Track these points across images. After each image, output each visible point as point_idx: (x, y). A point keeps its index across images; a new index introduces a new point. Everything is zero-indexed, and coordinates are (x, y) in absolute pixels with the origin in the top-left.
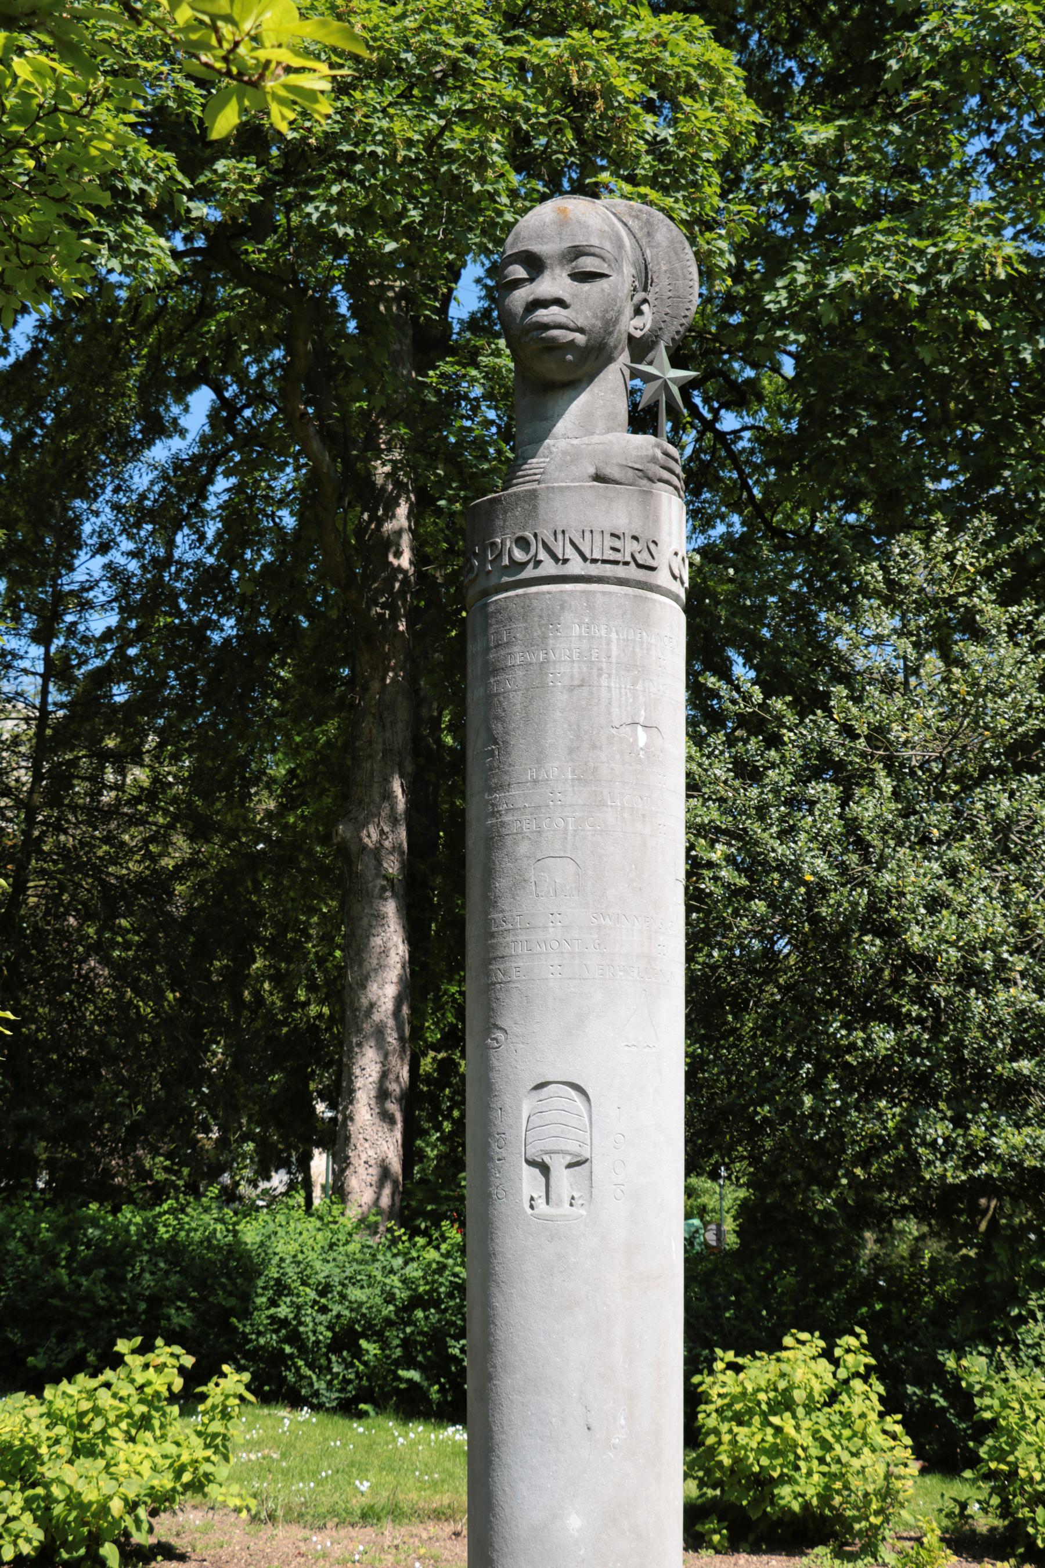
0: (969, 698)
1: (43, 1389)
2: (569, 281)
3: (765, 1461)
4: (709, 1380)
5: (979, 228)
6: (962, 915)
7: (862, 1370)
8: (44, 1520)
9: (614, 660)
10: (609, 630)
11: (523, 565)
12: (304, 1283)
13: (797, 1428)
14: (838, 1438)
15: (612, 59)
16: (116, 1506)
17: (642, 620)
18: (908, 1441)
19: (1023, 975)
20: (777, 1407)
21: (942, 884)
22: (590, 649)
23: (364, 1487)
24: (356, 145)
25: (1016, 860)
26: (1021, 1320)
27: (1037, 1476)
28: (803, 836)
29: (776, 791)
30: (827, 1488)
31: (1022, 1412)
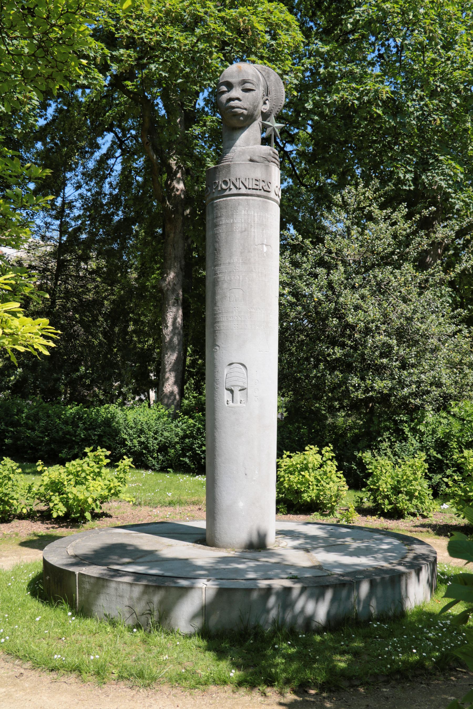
0: (370, 241)
1: (65, 464)
2: (241, 92)
3: (299, 486)
4: (281, 461)
5: (377, 81)
6: (365, 312)
7: (331, 457)
8: (66, 504)
9: (256, 222)
10: (254, 213)
11: (226, 190)
12: (149, 430)
13: (310, 475)
14: (322, 479)
15: (254, 17)
16: (90, 500)
17: (265, 209)
18: (345, 479)
19: (385, 331)
20: (302, 470)
21: (360, 301)
22: (248, 219)
23: (170, 494)
24: (168, 45)
25: (383, 294)
26: (381, 441)
27: (386, 490)
28: (314, 286)
29: (306, 270)
30: (319, 494)
31: (381, 470)
